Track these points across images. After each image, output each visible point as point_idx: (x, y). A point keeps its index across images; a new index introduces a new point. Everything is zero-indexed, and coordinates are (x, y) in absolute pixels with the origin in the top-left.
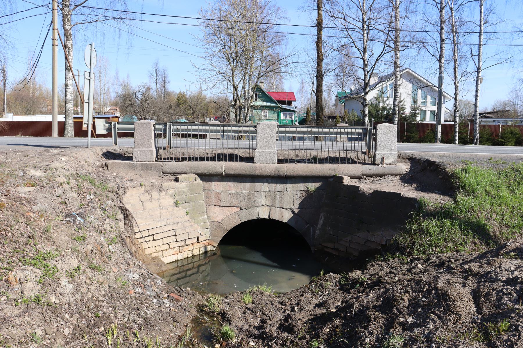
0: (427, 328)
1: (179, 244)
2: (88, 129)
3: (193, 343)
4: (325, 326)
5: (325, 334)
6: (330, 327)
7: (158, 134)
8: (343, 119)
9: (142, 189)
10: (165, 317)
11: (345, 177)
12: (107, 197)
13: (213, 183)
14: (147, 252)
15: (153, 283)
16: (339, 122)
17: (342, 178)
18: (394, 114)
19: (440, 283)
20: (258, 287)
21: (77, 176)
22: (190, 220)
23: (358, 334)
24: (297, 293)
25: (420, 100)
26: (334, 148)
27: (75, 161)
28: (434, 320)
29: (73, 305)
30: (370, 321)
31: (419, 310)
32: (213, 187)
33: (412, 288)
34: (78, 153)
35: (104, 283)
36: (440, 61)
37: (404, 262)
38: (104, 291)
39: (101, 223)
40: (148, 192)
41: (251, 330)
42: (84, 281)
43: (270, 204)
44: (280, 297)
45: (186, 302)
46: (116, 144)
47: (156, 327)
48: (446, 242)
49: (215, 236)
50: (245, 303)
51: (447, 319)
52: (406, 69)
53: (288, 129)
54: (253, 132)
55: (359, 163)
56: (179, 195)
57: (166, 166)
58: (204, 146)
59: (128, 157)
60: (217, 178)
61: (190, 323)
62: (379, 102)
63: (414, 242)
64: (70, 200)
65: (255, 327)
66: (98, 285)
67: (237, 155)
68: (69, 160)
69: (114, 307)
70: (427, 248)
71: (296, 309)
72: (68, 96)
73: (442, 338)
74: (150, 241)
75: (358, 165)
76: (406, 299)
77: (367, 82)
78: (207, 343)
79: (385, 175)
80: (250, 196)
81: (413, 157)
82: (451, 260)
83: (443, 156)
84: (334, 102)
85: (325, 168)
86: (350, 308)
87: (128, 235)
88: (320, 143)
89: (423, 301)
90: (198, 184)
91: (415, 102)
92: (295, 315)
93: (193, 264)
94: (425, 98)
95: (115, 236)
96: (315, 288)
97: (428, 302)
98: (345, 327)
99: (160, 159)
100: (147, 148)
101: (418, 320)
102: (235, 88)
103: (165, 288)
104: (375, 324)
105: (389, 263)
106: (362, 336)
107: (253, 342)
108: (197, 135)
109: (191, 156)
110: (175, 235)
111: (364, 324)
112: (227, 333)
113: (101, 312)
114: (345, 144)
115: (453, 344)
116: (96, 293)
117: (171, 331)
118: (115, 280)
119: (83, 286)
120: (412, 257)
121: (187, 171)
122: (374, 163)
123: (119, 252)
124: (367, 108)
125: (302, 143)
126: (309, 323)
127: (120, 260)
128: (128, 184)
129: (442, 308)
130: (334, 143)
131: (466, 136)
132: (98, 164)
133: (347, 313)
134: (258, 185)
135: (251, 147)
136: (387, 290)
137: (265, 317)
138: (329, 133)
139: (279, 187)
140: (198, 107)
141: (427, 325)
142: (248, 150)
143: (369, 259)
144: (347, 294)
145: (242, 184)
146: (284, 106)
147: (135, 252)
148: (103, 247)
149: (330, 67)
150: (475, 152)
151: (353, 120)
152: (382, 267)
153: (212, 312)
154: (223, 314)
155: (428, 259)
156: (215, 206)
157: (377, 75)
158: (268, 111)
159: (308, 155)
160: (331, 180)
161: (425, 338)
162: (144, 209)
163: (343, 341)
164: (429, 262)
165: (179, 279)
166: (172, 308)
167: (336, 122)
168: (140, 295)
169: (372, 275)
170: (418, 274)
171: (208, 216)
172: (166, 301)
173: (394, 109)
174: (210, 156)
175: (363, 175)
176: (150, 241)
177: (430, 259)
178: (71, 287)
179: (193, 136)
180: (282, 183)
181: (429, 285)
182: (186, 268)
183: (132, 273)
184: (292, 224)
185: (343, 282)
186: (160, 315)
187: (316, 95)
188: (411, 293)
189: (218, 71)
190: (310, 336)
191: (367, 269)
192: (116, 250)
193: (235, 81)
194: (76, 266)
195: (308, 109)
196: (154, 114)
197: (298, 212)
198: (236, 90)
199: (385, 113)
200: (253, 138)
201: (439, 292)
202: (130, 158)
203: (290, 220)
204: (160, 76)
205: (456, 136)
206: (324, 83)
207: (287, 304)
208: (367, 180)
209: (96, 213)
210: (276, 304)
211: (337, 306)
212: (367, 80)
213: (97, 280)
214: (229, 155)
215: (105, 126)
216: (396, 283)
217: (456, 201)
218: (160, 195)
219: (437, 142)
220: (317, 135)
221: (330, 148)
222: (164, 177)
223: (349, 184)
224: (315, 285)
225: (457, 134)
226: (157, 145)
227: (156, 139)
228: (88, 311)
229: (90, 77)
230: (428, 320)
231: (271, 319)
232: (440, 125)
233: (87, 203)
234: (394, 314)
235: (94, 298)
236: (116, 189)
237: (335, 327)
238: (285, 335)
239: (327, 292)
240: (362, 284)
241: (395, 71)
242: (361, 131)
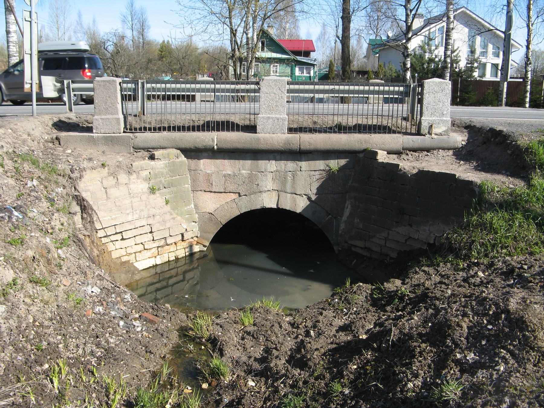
0: (495, 370)
1: (157, 244)
2: (32, 90)
3: (171, 382)
4: (351, 361)
5: (351, 373)
6: (358, 363)
7: (126, 95)
8: (377, 75)
9: (105, 171)
10: (135, 347)
11: (380, 152)
12: (56, 183)
14: (115, 255)
15: (119, 299)
16: (371, 79)
17: (376, 153)
18: (445, 67)
19: (512, 304)
20: (262, 302)
21: (14, 156)
22: (172, 211)
23: (398, 375)
24: (314, 311)
25: (478, 50)
26: (365, 112)
27: (14, 135)
28: (506, 359)
29: (5, 334)
30: (414, 356)
31: (484, 343)
32: (202, 167)
33: (472, 309)
34: (19, 124)
35: (50, 302)
37: (458, 268)
38: (51, 312)
39: (47, 219)
40: (113, 174)
41: (251, 363)
42: (22, 300)
43: (279, 189)
44: (291, 315)
45: (164, 324)
46: (71, 110)
47: (122, 360)
48: (516, 242)
49: (205, 233)
50: (243, 324)
51: (524, 359)
52: (462, 8)
53: (302, 87)
54: (255, 91)
55: (399, 133)
56: (155, 178)
57: (137, 139)
58: (188, 111)
59: (88, 127)
60: (206, 154)
61: (169, 354)
62: (425, 52)
63: (473, 241)
64: (4, 188)
65: (256, 359)
66: (42, 304)
67: (233, 123)
68: (5, 134)
69: (64, 335)
70: (490, 248)
71: (312, 333)
72: (11, 47)
73: (518, 388)
74: (117, 240)
75: (397, 135)
76: (465, 326)
77: (409, 24)
78: (191, 382)
80: (251, 178)
81: (472, 125)
82: (524, 266)
83: (513, 124)
84: (365, 53)
85: (352, 139)
86: (386, 335)
87: (87, 233)
88: (346, 106)
89: (489, 330)
90: (181, 162)
91: (473, 52)
92: (310, 343)
93: (176, 269)
94: (485, 47)
95: (66, 236)
96: (339, 303)
97: (496, 331)
98: (379, 363)
99: (129, 129)
101: (483, 358)
102: (233, 34)
103: (136, 305)
104: (420, 362)
105: (439, 269)
106: (403, 379)
107: (253, 381)
108: (174, 96)
109: (172, 125)
110: (151, 232)
111: (406, 360)
112: (218, 369)
113: (45, 343)
114: (380, 108)
115: (535, 398)
116: (39, 315)
117: (143, 366)
118: (66, 297)
119: (21, 306)
120: (470, 262)
121: (166, 145)
122: (419, 133)
123: (72, 258)
124: (409, 59)
125: (321, 106)
126: (329, 355)
127: (74, 269)
128: (85, 164)
129: (516, 342)
130: (366, 106)
131: (539, 98)
132: (46, 138)
133: (381, 343)
134: (262, 164)
135: (252, 111)
136: (438, 311)
137: (270, 345)
138: (358, 92)
139: (290, 165)
140: (186, 60)
141: (496, 365)
142: (248, 116)
143: (411, 264)
144: (382, 313)
145: (241, 161)
146: (299, 58)
147: (98, 256)
148: (49, 252)
149: (360, 4)
151: (391, 75)
152: (429, 274)
153: (199, 338)
154: (213, 341)
155: (491, 265)
156: (205, 191)
157: (421, 16)
158: (278, 65)
159: (330, 122)
160: (361, 155)
161: (493, 387)
162: (108, 198)
163: (376, 385)
164: (493, 268)
165: (158, 290)
166: (145, 333)
167: (368, 79)
168: (101, 316)
169: (415, 286)
170: (478, 286)
171: (195, 206)
172: (137, 323)
173: (445, 61)
174: (196, 124)
175: (403, 149)
176: (117, 240)
177: (495, 265)
178: (4, 310)
179: (179, 98)
181: (497, 305)
182: (167, 275)
183: (90, 286)
184: (308, 215)
185: (376, 295)
186: (128, 343)
187: (341, 42)
188: (471, 316)
189: (210, 10)
190: (330, 374)
191: (409, 278)
192: (68, 255)
193: (233, 25)
194: (10, 280)
195: (331, 62)
196: (128, 71)
198: (235, 35)
199: (433, 66)
200: (255, 100)
201: (512, 316)
202: (89, 130)
204: (136, 21)
205: (526, 97)
206: (352, 25)
207: (300, 326)
208: (410, 156)
209: (41, 205)
210: (286, 326)
211: (369, 330)
212: (410, 22)
213: (40, 298)
214: (223, 122)
215: (55, 86)
216: (449, 298)
217: (530, 186)
218: (129, 179)
219: (501, 105)
220: (342, 95)
221: (360, 112)
222: (135, 153)
223: (386, 161)
224: (338, 299)
225: (528, 95)
226: (124, 110)
227: (124, 103)
228: (26, 341)
229: (30, 17)
230: (497, 359)
231: (278, 348)
232: (506, 83)
233: (28, 191)
234: (447, 346)
235: (37, 324)
236: (68, 172)
237: (365, 363)
238: (296, 372)
239: (355, 309)
240: (402, 298)
241: (448, 10)
242: (402, 89)
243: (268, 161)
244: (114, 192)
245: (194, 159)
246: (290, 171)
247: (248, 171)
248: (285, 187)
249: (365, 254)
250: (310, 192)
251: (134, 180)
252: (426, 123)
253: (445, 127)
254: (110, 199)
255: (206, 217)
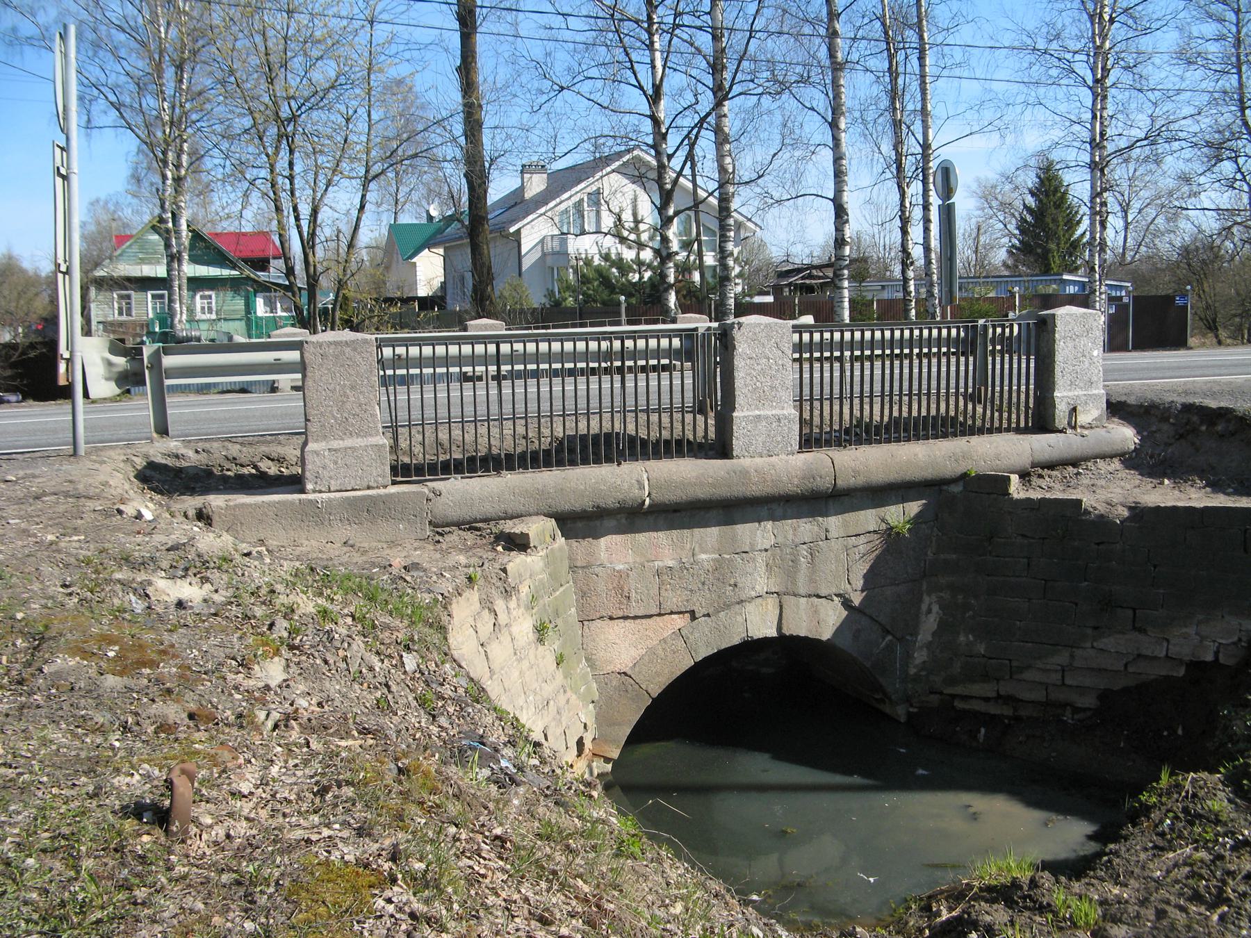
13: (602, 539)
32: (603, 556)
36: (834, 125)
46: (163, 430)
60: (611, 523)
77: (668, 186)
79: (1087, 459)
80: (721, 571)
100: (358, 435)
139: (805, 528)
145: (696, 531)
150: (1206, 372)
156: (611, 618)
158: (213, 294)
180: (813, 516)
184: (845, 644)
197: (861, 603)
202: (295, 483)
203: (839, 631)
215: (110, 364)
243: (757, 524)
245: (584, 538)
246: (805, 543)
247: (714, 553)
248: (794, 583)
249: (998, 712)
250: (848, 586)
252: (1063, 403)
255: (614, 683)
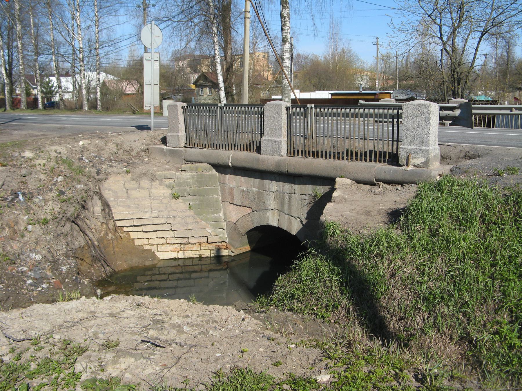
43: (280, 209)
60: (229, 171)
121: (201, 160)
139: (286, 187)
145: (252, 179)
162: (128, 197)
180: (289, 183)
182: (191, 269)
218: (152, 185)
243: (270, 181)
244: (135, 194)
251: (156, 186)
252: (404, 152)
253: (424, 157)
254: (129, 198)
